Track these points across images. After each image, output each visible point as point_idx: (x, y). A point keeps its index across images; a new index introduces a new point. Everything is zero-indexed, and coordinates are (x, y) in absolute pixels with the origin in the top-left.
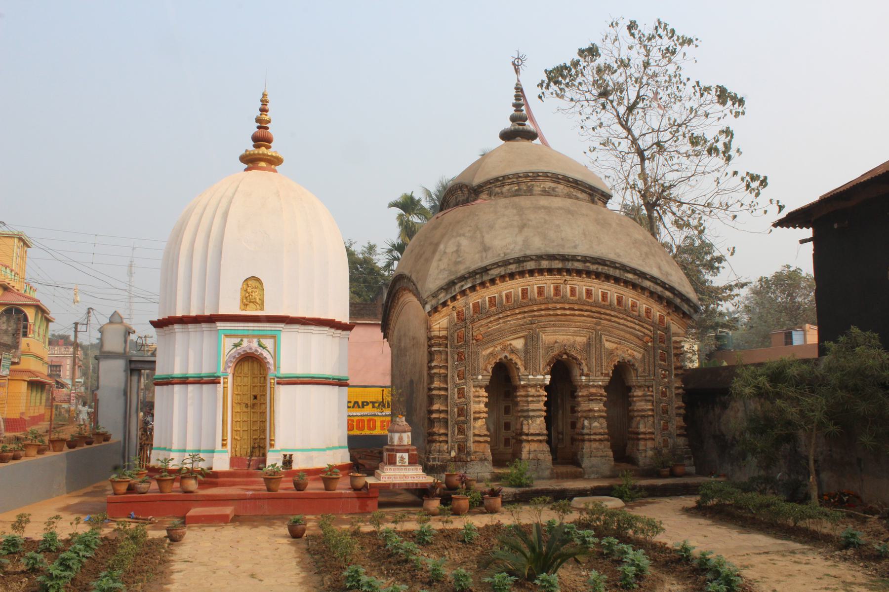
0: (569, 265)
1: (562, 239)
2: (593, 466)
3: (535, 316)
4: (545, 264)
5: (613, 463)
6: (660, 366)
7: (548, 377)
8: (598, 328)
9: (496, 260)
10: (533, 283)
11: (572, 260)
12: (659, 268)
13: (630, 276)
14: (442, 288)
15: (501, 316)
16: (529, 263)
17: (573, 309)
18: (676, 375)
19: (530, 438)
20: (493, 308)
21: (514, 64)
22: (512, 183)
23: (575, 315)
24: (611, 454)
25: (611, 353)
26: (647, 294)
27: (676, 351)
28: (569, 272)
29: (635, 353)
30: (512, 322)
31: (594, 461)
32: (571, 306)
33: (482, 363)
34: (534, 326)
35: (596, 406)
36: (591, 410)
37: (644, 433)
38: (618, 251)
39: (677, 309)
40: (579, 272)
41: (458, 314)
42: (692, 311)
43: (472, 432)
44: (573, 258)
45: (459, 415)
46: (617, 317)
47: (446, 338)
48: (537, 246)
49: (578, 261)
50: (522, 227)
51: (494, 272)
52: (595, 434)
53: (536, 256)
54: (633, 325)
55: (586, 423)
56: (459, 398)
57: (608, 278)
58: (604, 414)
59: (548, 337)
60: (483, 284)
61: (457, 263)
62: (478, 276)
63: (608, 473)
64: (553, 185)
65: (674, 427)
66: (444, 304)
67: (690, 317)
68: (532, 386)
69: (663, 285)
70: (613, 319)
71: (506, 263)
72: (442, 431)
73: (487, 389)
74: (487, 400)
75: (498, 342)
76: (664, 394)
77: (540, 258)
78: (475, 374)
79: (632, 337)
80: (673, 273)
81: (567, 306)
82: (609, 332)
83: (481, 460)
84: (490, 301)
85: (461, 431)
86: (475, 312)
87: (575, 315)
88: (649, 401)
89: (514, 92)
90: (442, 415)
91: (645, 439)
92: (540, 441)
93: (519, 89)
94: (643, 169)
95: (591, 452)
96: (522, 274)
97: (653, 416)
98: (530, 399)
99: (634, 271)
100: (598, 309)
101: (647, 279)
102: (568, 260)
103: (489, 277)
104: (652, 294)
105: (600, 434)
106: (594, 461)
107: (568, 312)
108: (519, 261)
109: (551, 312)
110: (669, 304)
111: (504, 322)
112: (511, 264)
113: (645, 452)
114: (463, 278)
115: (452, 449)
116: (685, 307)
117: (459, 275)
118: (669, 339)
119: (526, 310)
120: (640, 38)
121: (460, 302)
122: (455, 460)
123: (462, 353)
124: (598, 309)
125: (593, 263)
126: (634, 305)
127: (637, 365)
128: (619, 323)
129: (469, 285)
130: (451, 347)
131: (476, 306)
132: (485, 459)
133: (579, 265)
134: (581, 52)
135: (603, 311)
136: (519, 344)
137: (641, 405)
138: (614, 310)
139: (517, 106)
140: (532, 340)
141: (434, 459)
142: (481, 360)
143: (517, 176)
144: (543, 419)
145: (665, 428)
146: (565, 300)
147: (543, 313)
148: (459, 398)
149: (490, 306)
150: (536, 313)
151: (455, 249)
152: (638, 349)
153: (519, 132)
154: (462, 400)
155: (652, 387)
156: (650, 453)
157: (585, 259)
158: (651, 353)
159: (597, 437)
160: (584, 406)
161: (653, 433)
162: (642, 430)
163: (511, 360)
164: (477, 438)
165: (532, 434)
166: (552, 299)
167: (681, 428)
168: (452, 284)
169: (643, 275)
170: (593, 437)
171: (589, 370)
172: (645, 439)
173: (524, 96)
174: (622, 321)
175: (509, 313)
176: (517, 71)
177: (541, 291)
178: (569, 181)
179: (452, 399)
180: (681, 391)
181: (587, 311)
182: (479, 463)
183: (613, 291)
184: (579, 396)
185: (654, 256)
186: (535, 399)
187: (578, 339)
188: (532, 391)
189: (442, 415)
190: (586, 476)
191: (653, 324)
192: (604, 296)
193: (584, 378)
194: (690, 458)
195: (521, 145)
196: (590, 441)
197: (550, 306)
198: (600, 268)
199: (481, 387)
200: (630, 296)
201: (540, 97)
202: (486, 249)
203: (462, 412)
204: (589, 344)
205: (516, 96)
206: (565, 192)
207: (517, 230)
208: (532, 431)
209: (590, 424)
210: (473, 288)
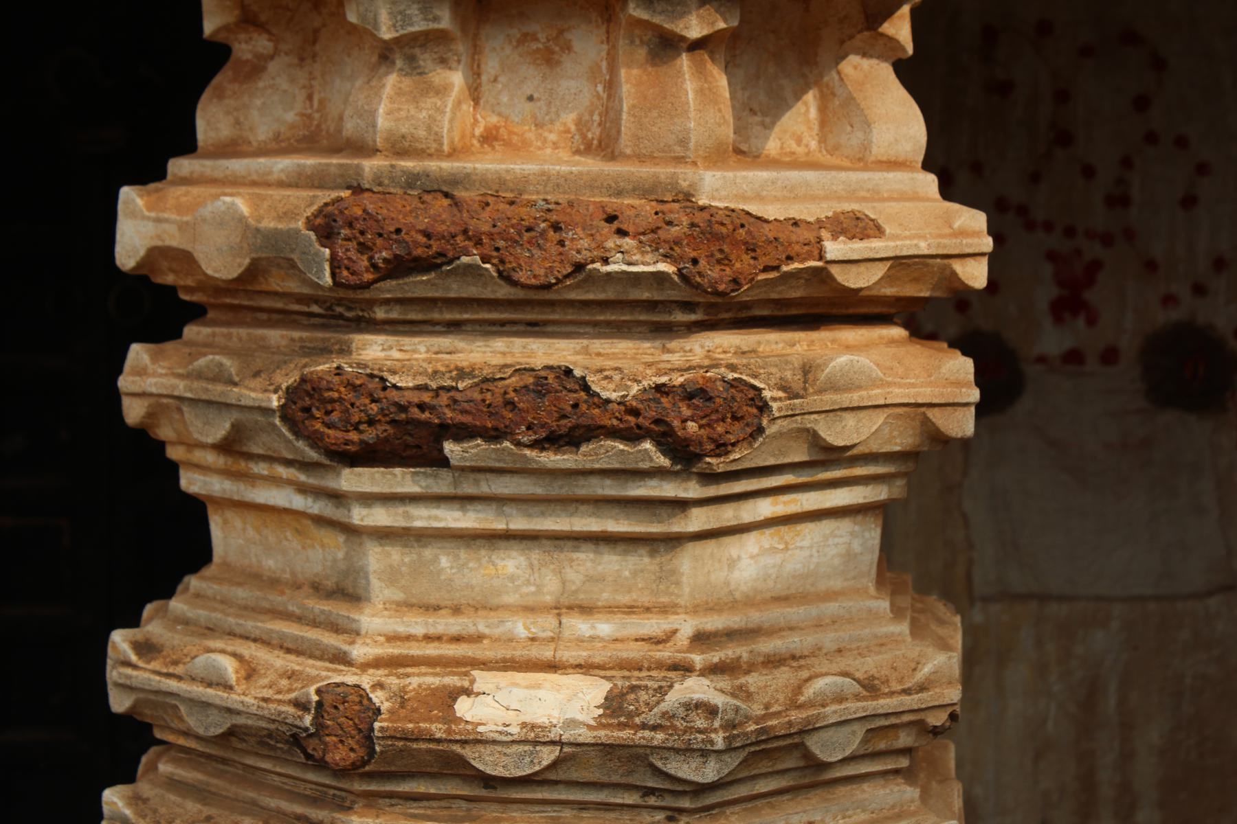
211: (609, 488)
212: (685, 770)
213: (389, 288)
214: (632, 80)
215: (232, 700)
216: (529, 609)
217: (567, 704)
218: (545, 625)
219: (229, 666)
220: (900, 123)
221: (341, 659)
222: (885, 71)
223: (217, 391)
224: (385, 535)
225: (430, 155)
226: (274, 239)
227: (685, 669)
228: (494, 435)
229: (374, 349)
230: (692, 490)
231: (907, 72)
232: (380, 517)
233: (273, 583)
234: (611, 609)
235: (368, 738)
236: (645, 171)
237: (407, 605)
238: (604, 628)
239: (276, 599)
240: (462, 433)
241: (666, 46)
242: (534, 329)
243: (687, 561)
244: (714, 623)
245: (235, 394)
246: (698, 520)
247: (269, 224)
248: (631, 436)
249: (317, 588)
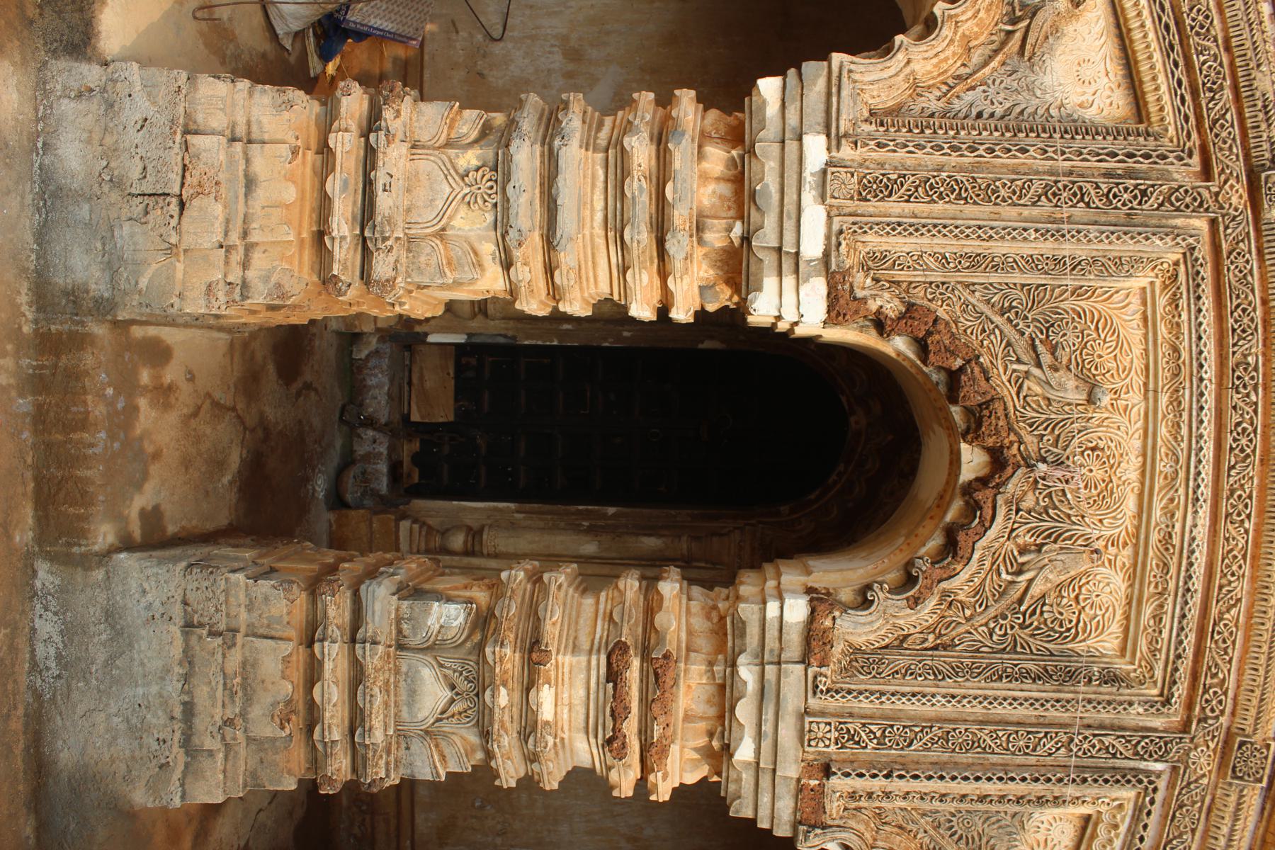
2: (120, 635)
7: (792, 305)
8: (1204, 761)
19: (345, 144)
31: (159, 646)
34: (1237, 195)
35: (565, 697)
36: (534, 650)
52: (357, 677)
55: (447, 617)
63: (66, 754)
95: (228, 635)
105: (357, 720)
144: (491, 282)
159: (332, 694)
160: (573, 615)
170: (334, 656)
171: (864, 660)
184: (650, 583)
186: (639, 189)
187: (1109, 585)
188: (700, 177)
190: (46, 575)
193: (797, 610)
196: (311, 635)
204: (1066, 674)
208: (394, 158)
209: (432, 648)
211: (600, 721)
212: (531, 740)
213: (651, 671)
214: (703, 726)
215: (548, 621)
216: (570, 697)
217: (546, 712)
218: (566, 701)
219: (554, 619)
220: (691, 778)
221: (558, 653)
222: (705, 774)
223: (626, 618)
224: (589, 662)
225: (746, 239)
226: (664, 639)
227: (555, 737)
228: (614, 696)
229: (636, 663)
230: (600, 742)
231: (706, 778)
232: (594, 663)
233: (577, 623)
234: (570, 717)
235: (539, 663)
236: (679, 731)
237: (571, 666)
238: (566, 716)
239: (572, 626)
240: (615, 688)
241: (711, 735)
242: (641, 700)
243: (582, 736)
244: (566, 741)
245: (625, 624)
246: (592, 740)
247: (668, 637)
248: (613, 730)
249: (576, 638)
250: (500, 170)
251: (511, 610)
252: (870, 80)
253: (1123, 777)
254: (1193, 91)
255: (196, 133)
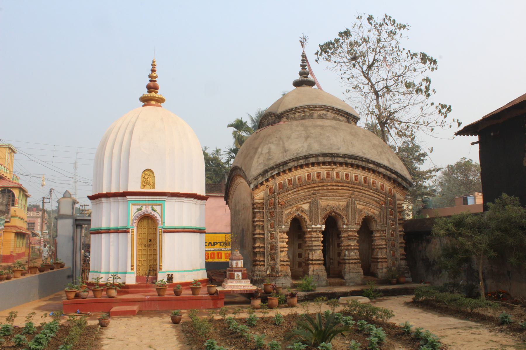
0: (335, 160)
1: (331, 145)
2: (351, 278)
3: (315, 190)
4: (321, 159)
5: (363, 276)
6: (390, 218)
7: (324, 226)
8: (353, 196)
9: (292, 157)
10: (314, 171)
11: (337, 157)
12: (389, 160)
13: (371, 166)
14: (260, 174)
15: (295, 190)
16: (311, 159)
17: (338, 186)
18: (399, 224)
19: (314, 262)
20: (291, 186)
21: (301, 41)
22: (301, 112)
23: (338, 189)
24: (362, 271)
25: (361, 211)
26: (381, 176)
27: (399, 210)
28: (335, 163)
29: (375, 211)
30: (302, 194)
31: (352, 275)
32: (337, 184)
33: (284, 218)
34: (315, 196)
35: (353, 243)
37: (381, 258)
38: (364, 151)
39: (399, 185)
40: (341, 164)
41: (270, 190)
42: (408, 185)
43: (279, 259)
44: (338, 156)
45: (271, 249)
46: (364, 190)
47: (263, 204)
48: (316, 148)
49: (340, 157)
50: (307, 138)
51: (291, 165)
52: (352, 259)
53: (316, 154)
54: (373, 195)
55: (347, 253)
56: (271, 239)
57: (358, 167)
58: (357, 248)
59: (323, 203)
60: (284, 172)
61: (269, 159)
62: (281, 167)
64: (325, 112)
65: (399, 254)
66: (262, 184)
67: (407, 189)
68: (314, 232)
69: (391, 170)
70: (362, 191)
71: (298, 159)
72: (261, 259)
73: (288, 234)
74: (288, 240)
75: (294, 206)
76: (392, 235)
77: (318, 155)
78: (280, 225)
79: (373, 202)
80: (397, 163)
81: (334, 184)
82: (359, 199)
83: (285, 276)
84: (289, 182)
85: (273, 259)
86: (280, 188)
87: (338, 189)
88: (384, 239)
89: (301, 58)
90: (261, 250)
91: (382, 262)
92: (320, 264)
93: (304, 56)
94: (378, 102)
95: (350, 270)
96: (307, 165)
97: (386, 248)
98: (313, 239)
99: (373, 163)
100: (352, 185)
101: (381, 167)
102: (334, 157)
103: (288, 168)
104: (384, 176)
105: (355, 259)
106: (352, 275)
107: (335, 187)
108: (305, 158)
109: (325, 188)
110: (395, 181)
111: (297, 194)
112: (301, 159)
113: (382, 270)
114: (272, 168)
115: (267, 269)
116: (404, 184)
117: (270, 166)
118: (395, 202)
119: (310, 186)
120: (375, 25)
121: (271, 183)
122: (269, 276)
123: (273, 213)
124: (352, 185)
125: (349, 158)
126: (374, 183)
127: (376, 218)
128: (365, 194)
129: (276, 172)
130: (266, 209)
131: (280, 184)
132: (287, 275)
133: (341, 160)
134: (340, 34)
135: (355, 186)
136: (306, 207)
137: (379, 242)
138: (362, 186)
139: (303, 66)
140: (314, 204)
141: (257, 276)
142: (284, 217)
143: (303, 107)
145: (394, 255)
146: (332, 180)
147: (320, 188)
148: (271, 239)
149: (289, 185)
150: (316, 188)
151: (267, 151)
152: (377, 208)
153: (304, 81)
154: (273, 240)
155: (385, 231)
156: (385, 270)
157: (344, 156)
158: (385, 211)
159: (353, 261)
160: (345, 243)
161: (386, 258)
162: (380, 256)
163: (302, 216)
164: (282, 263)
165: (315, 260)
166: (325, 180)
167: (403, 255)
168: (266, 172)
169: (379, 165)
170: (351, 261)
171: (348, 221)
172: (382, 262)
173: (307, 61)
174: (367, 192)
175: (300, 188)
176: (303, 46)
177: (318, 175)
178: (334, 110)
179: (267, 240)
180: (402, 233)
181: (346, 186)
182: (284, 278)
183: (361, 175)
185: (385, 153)
186: (316, 239)
187: (341, 203)
188: (314, 235)
189: (261, 250)
190: (347, 285)
191: (385, 194)
192: (356, 177)
193: (345, 226)
194: (408, 273)
195: (305, 89)
196: (349, 263)
197: (324, 184)
198: (354, 161)
199: (284, 233)
200: (371, 178)
201: (316, 61)
202: (285, 151)
203: (273, 247)
204: (347, 206)
205: (302, 60)
206: (332, 116)
207: (304, 139)
208: (314, 258)
209: (349, 254)
210: (278, 174)
250: (315, 250)
251: (346, 248)
252: (308, 222)
253: (355, 202)
254: (308, 198)
255: (394, 113)
